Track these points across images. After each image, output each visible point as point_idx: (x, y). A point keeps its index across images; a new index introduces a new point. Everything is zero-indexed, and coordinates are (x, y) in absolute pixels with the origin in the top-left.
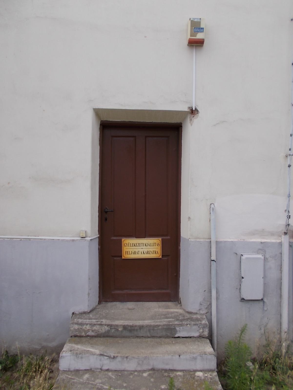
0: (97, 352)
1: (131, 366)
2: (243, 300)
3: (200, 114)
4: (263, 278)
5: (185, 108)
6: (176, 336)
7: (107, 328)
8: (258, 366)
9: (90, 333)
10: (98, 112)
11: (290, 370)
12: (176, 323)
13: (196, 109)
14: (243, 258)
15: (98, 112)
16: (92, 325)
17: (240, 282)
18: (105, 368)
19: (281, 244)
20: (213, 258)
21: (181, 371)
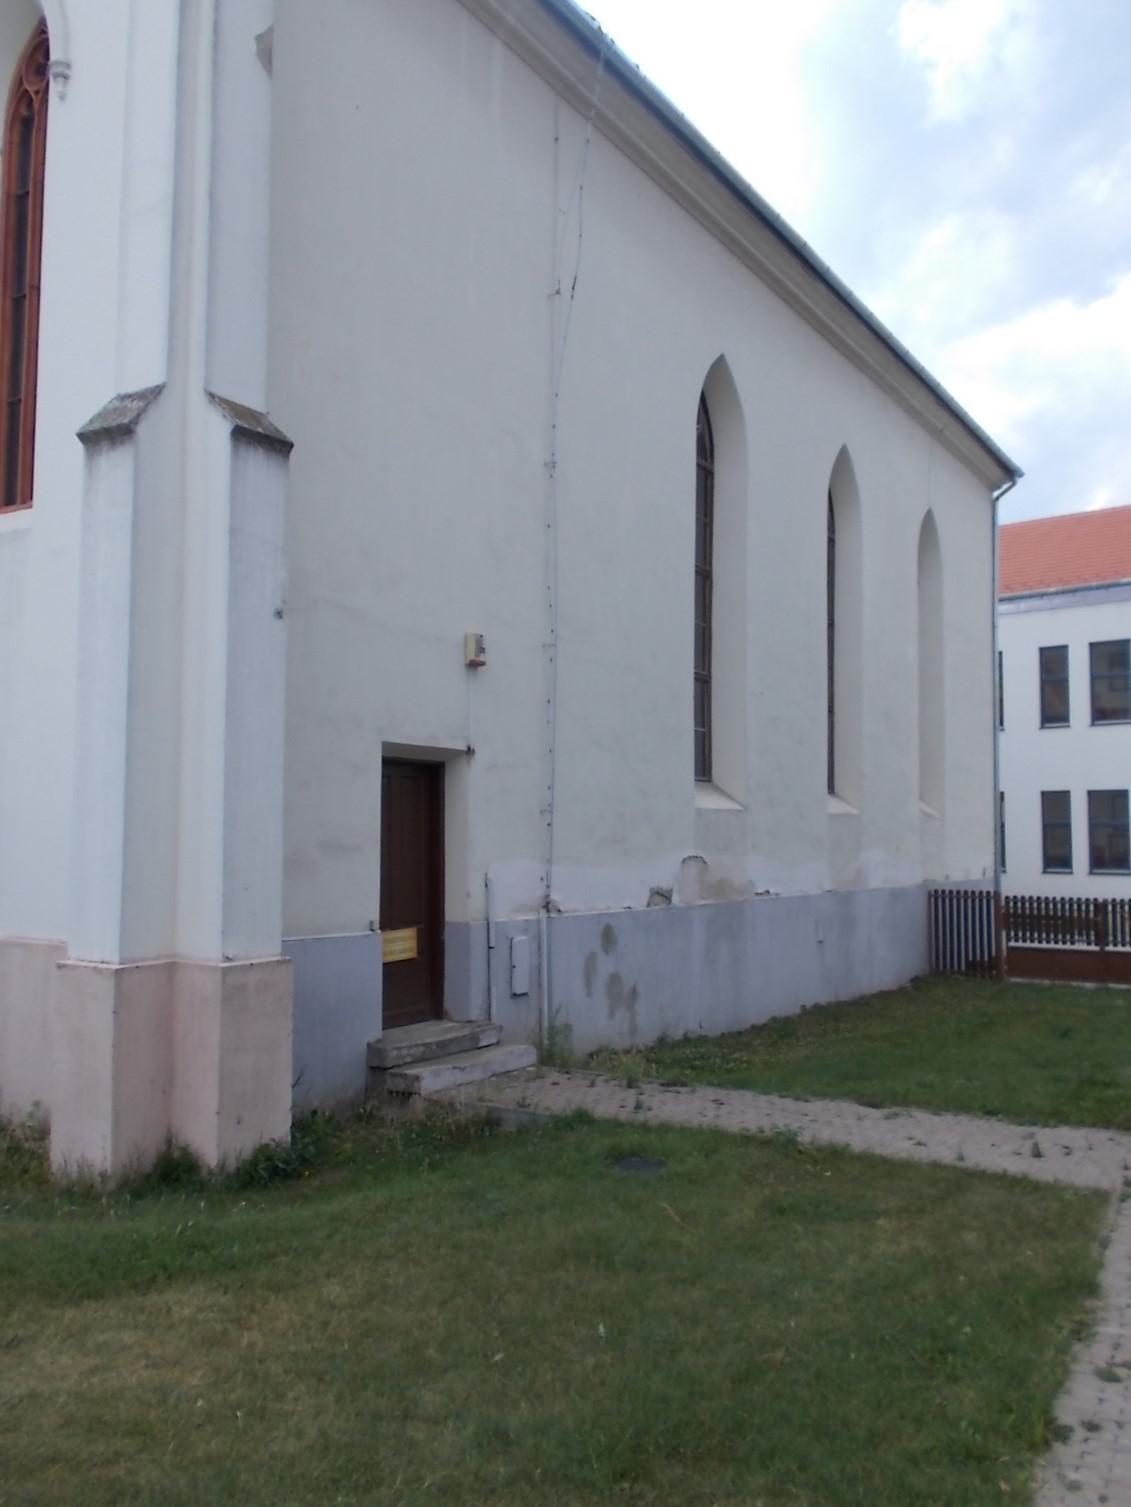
0: (450, 1066)
1: (477, 1075)
2: (515, 996)
3: (476, 756)
4: (279, 614)
5: (461, 746)
6: (481, 1045)
7: (421, 1049)
8: (52, 1174)
9: (408, 1060)
10: (386, 746)
11: (545, 1065)
12: (479, 1029)
13: (474, 751)
14: (515, 940)
15: (386, 746)
16: (410, 1047)
17: (511, 972)
18: (459, 1082)
19: (539, 921)
20: (492, 945)
21: (516, 1070)
